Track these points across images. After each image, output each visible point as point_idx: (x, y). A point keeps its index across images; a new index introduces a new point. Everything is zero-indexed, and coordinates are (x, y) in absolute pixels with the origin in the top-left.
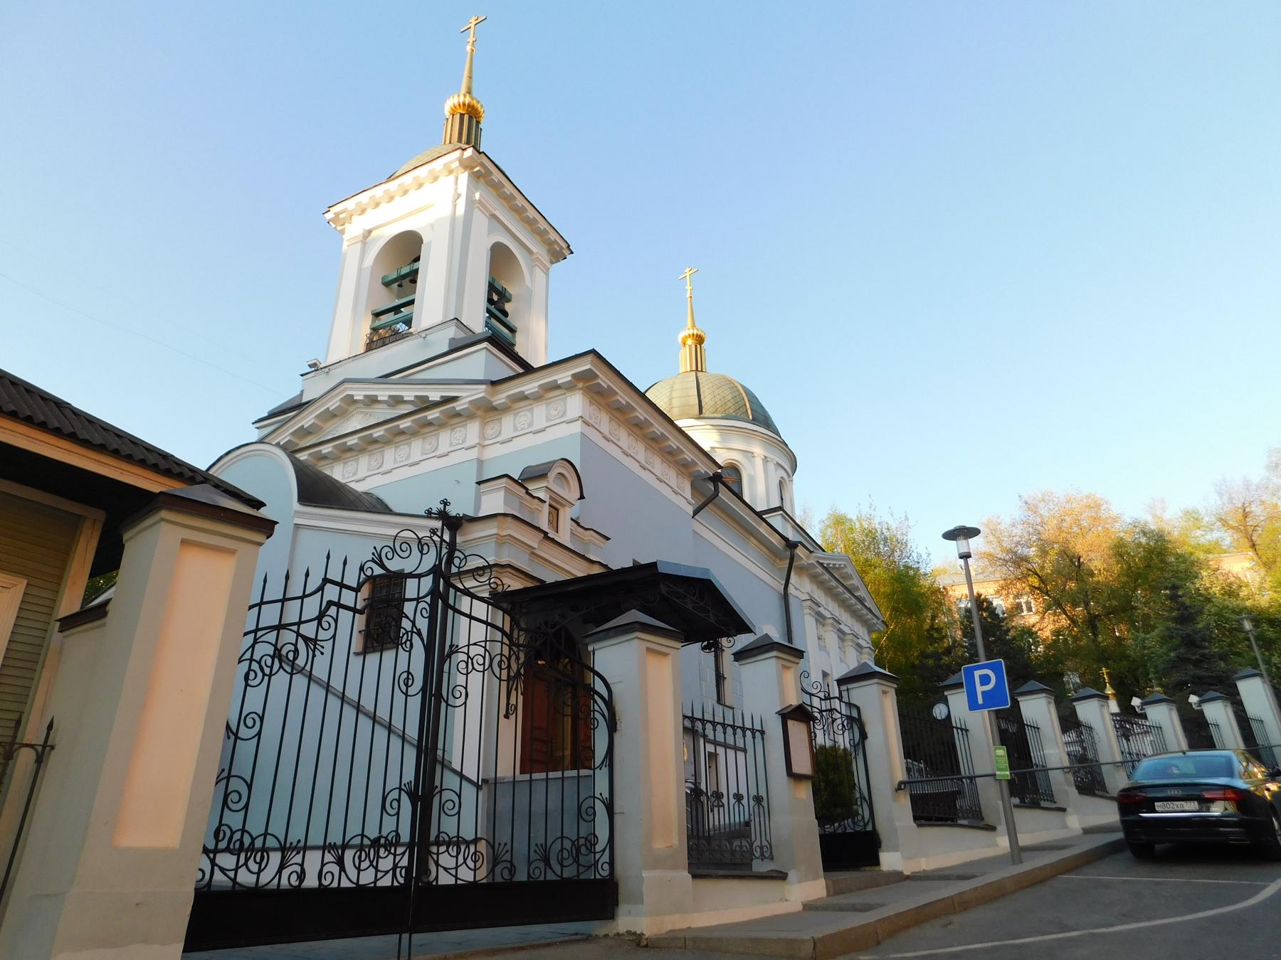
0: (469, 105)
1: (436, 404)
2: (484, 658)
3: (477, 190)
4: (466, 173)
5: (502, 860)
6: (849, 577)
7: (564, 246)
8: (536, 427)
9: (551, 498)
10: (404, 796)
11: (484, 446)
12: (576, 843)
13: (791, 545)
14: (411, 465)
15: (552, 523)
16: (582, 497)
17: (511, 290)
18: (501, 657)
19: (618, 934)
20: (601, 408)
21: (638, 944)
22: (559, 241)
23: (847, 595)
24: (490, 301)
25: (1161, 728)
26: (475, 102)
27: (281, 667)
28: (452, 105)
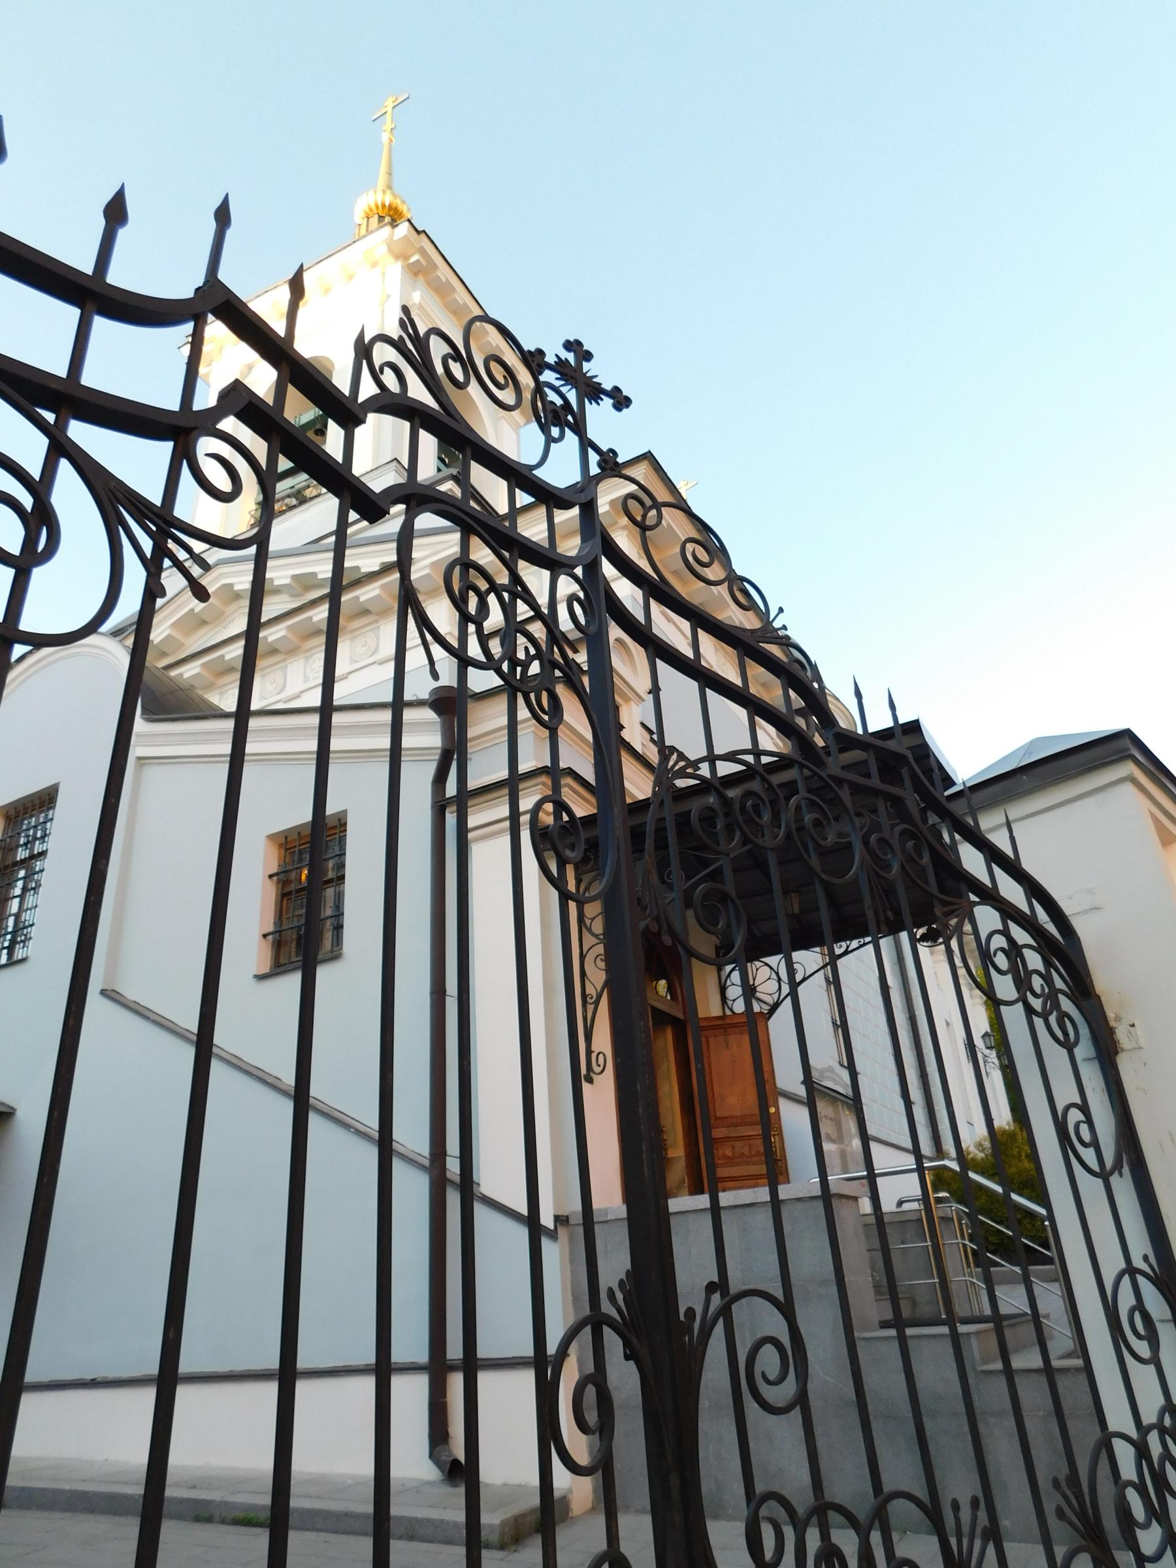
0: (390, 206)
3: (414, 290)
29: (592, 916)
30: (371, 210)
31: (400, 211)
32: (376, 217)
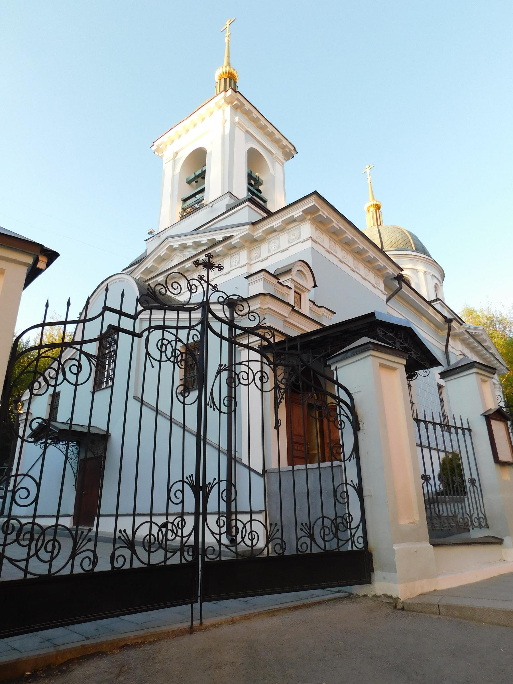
0: (228, 72)
1: (220, 242)
2: (248, 374)
3: (236, 117)
4: (229, 106)
5: (275, 537)
6: (485, 341)
7: (292, 148)
8: (282, 248)
9: (295, 286)
10: (187, 488)
11: (251, 265)
12: (335, 521)
13: (448, 321)
15: (297, 303)
16: (315, 286)
17: (262, 178)
18: (262, 374)
19: (375, 596)
20: (323, 233)
21: (395, 607)
22: (288, 145)
23: (485, 352)
24: (250, 184)
26: (232, 70)
27: (65, 379)
28: (219, 75)
29: (279, 375)
30: (221, 75)
31: (233, 74)
32: (223, 79)
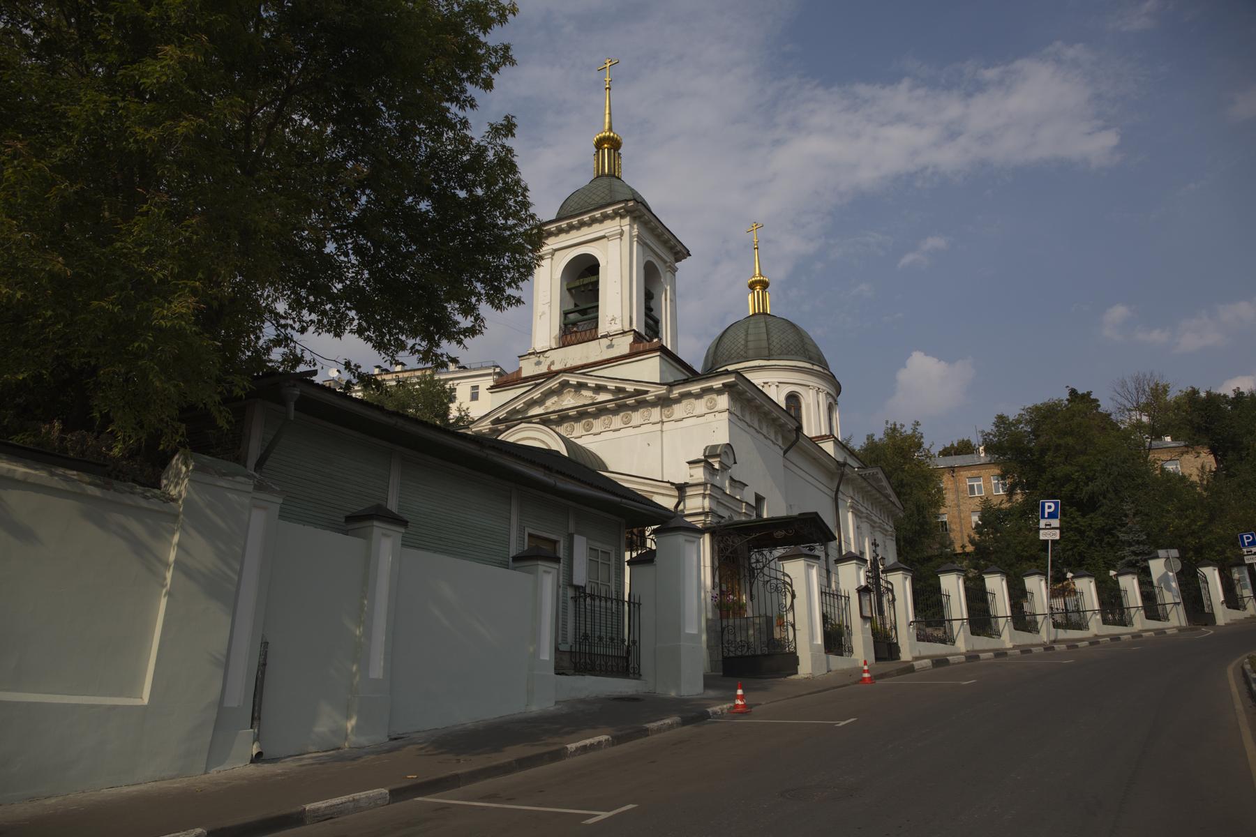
1: (631, 395)
14: (614, 431)
25: (949, 596)
